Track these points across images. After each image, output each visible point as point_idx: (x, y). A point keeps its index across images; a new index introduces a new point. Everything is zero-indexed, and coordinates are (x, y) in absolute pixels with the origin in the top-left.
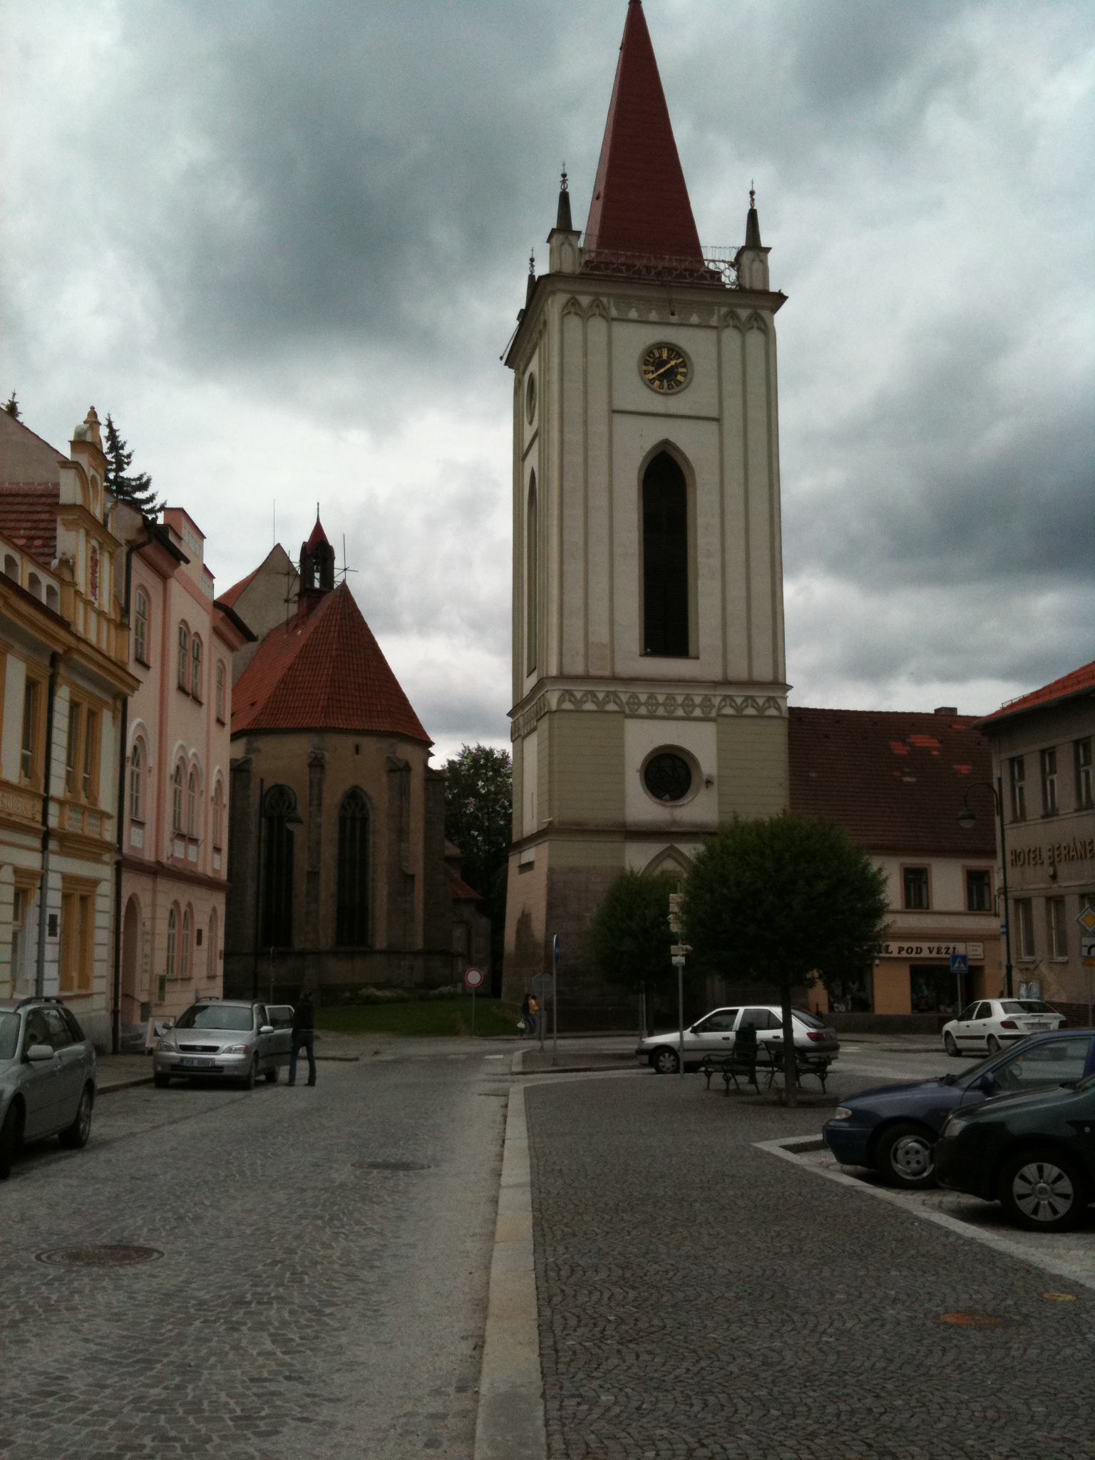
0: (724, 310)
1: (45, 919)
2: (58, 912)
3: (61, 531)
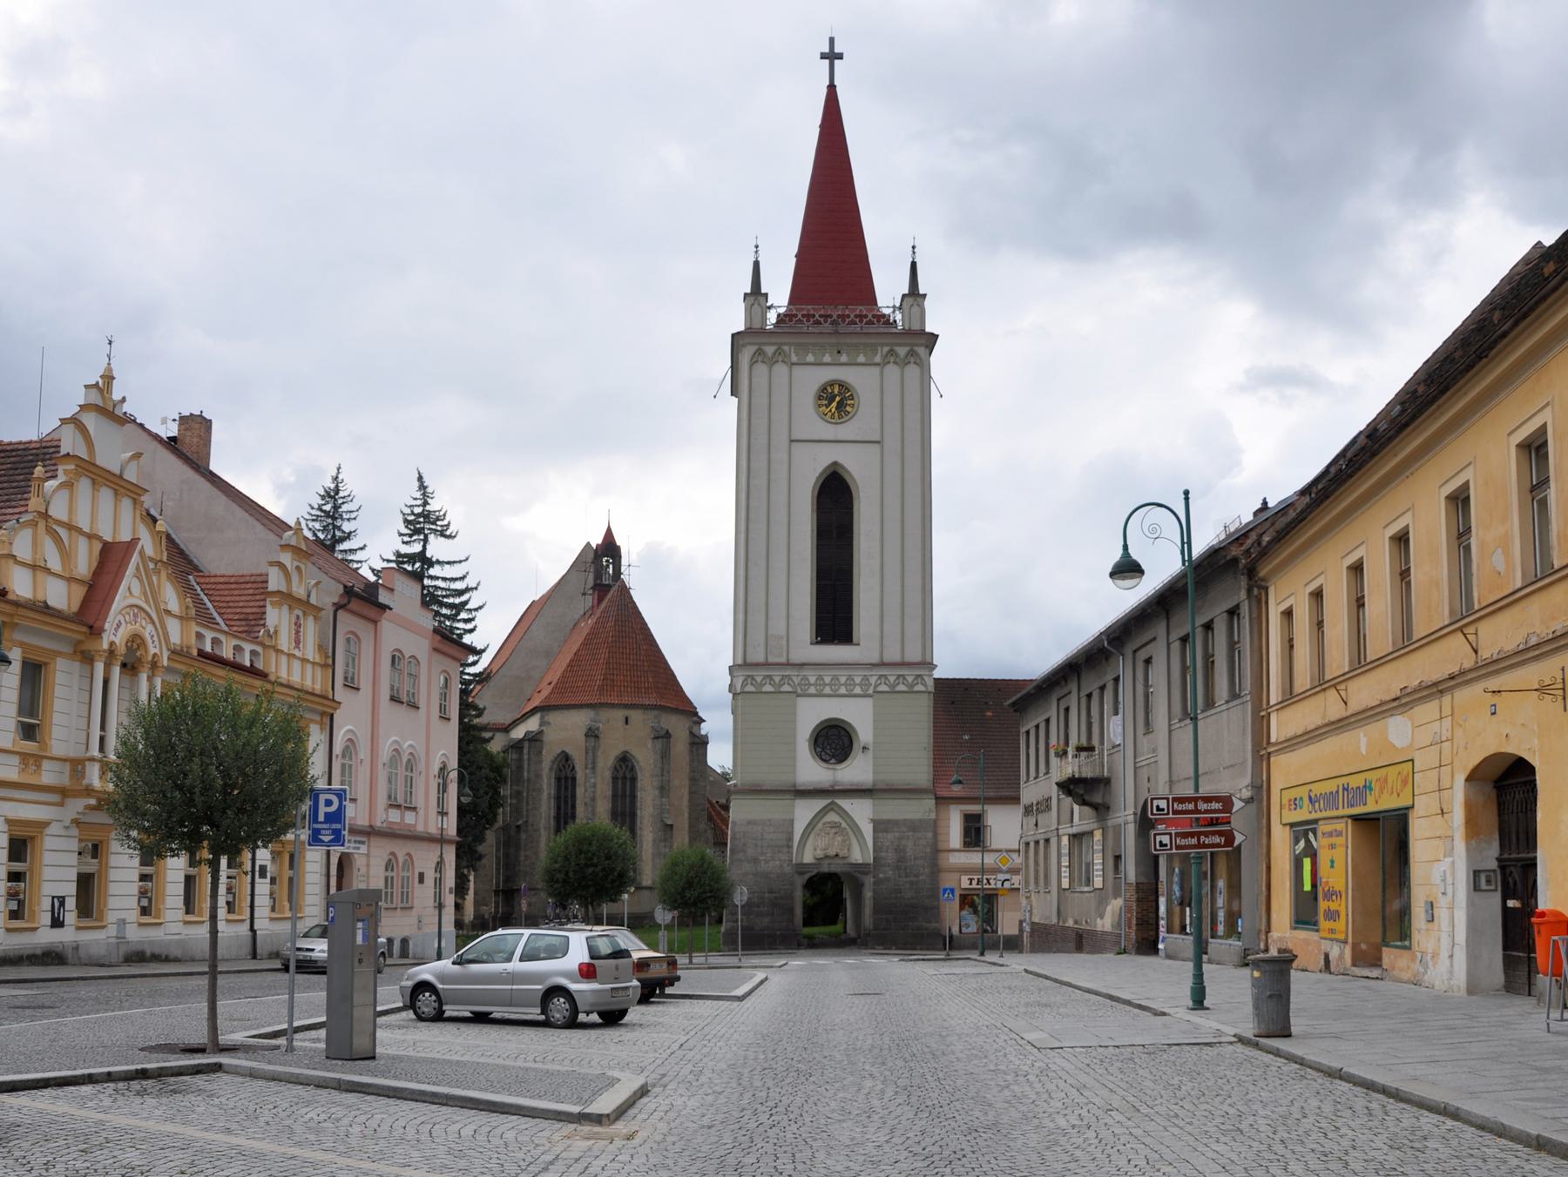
0: (886, 349)
2: (268, 864)
3: (269, 609)
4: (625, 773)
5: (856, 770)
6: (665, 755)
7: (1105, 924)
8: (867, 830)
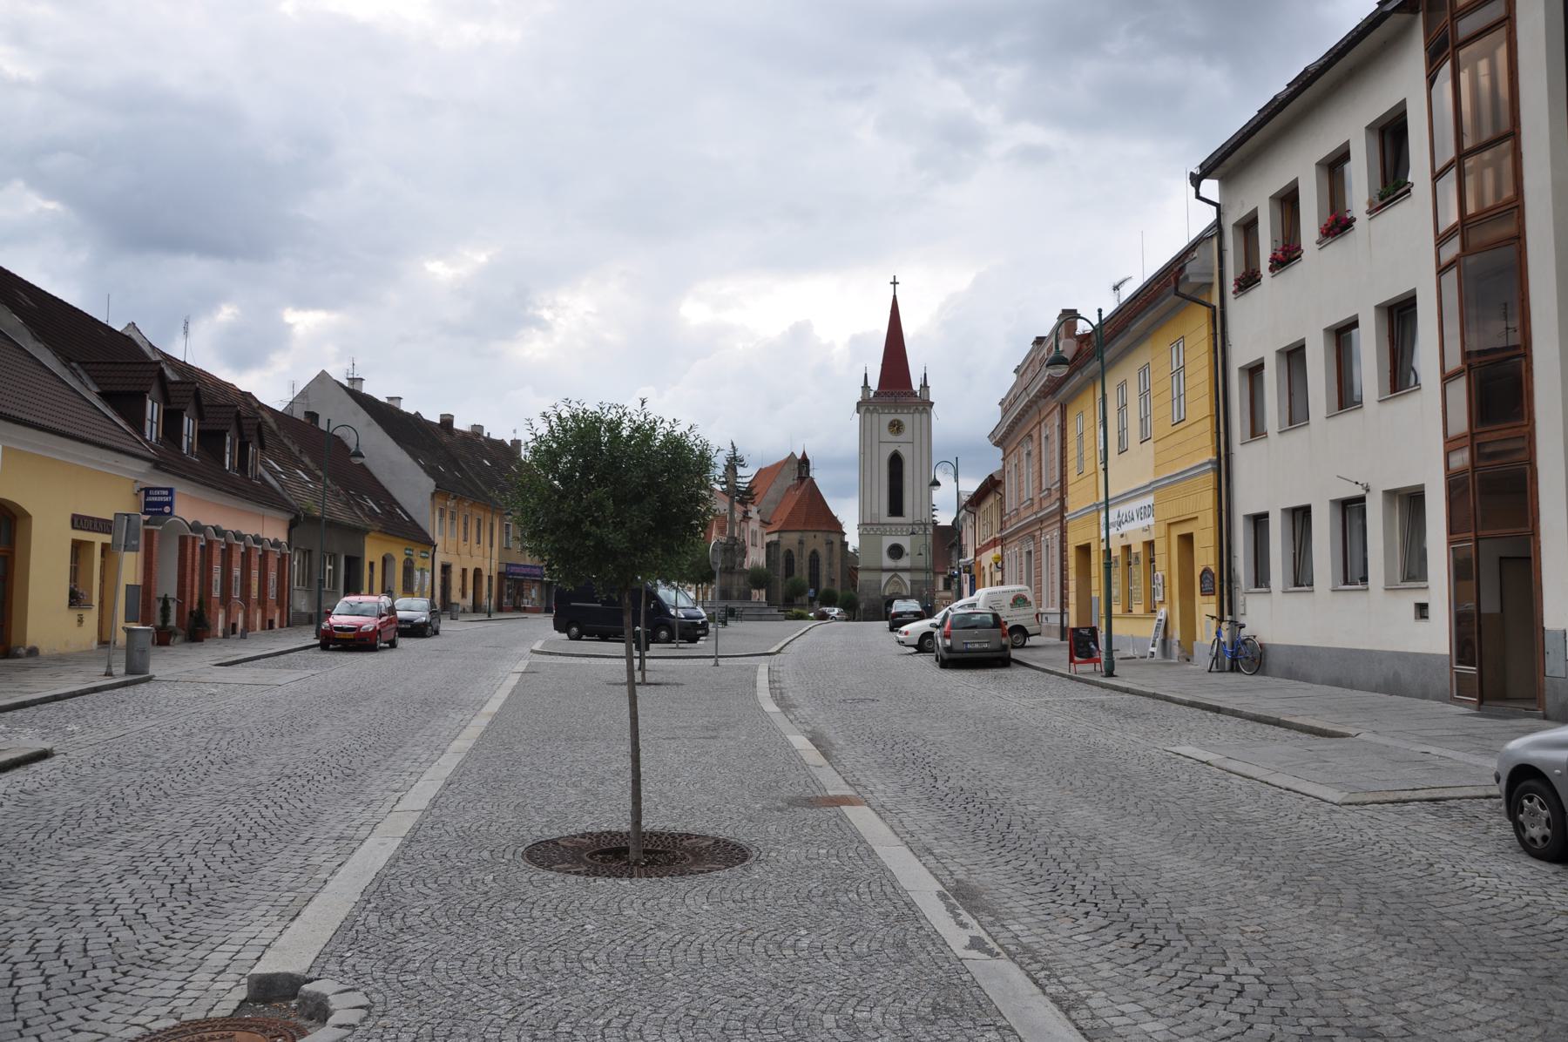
4: (814, 558)
5: (904, 562)
6: (831, 550)
8: (908, 583)
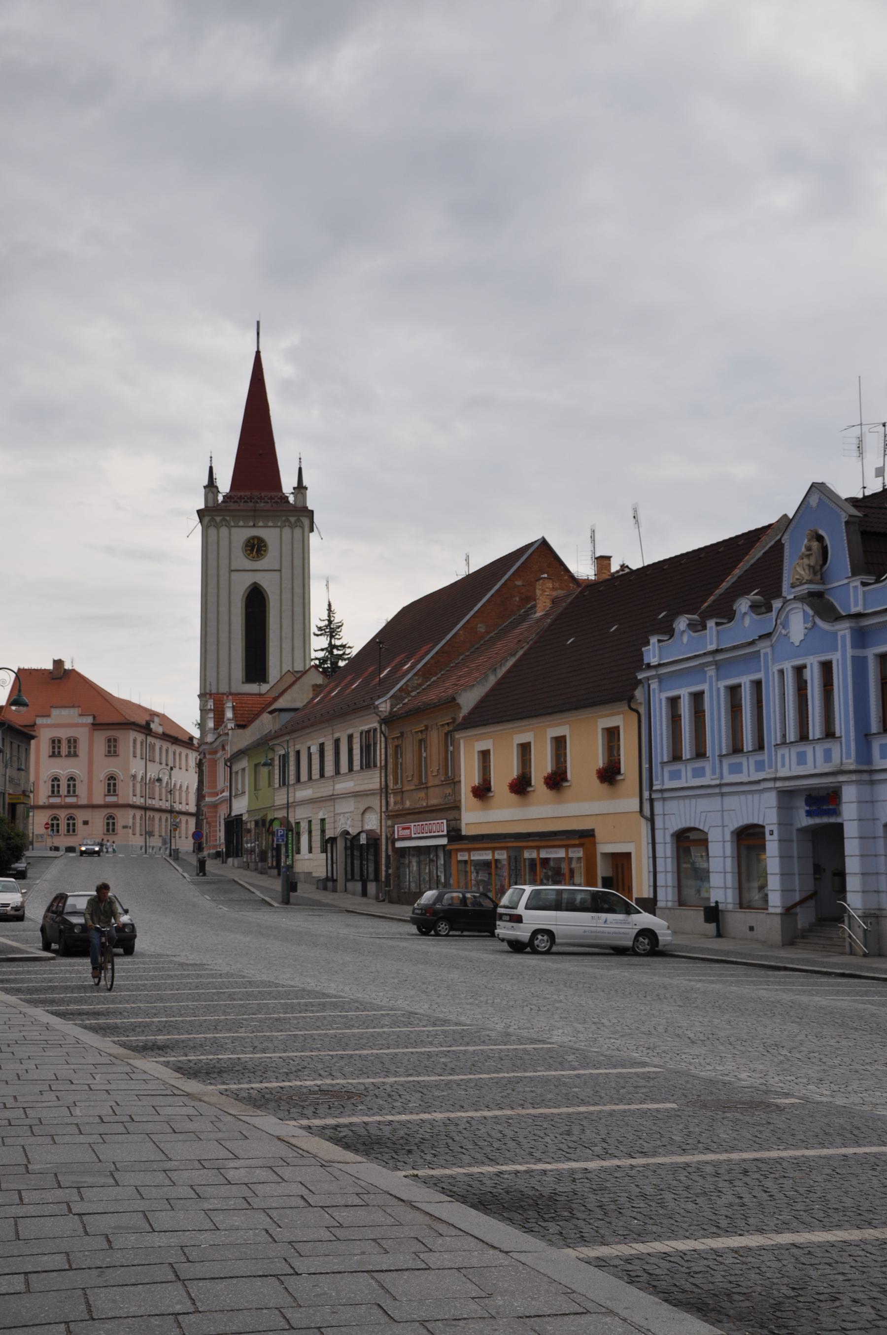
0: (284, 518)
1: (433, 877)
7: (688, 866)
